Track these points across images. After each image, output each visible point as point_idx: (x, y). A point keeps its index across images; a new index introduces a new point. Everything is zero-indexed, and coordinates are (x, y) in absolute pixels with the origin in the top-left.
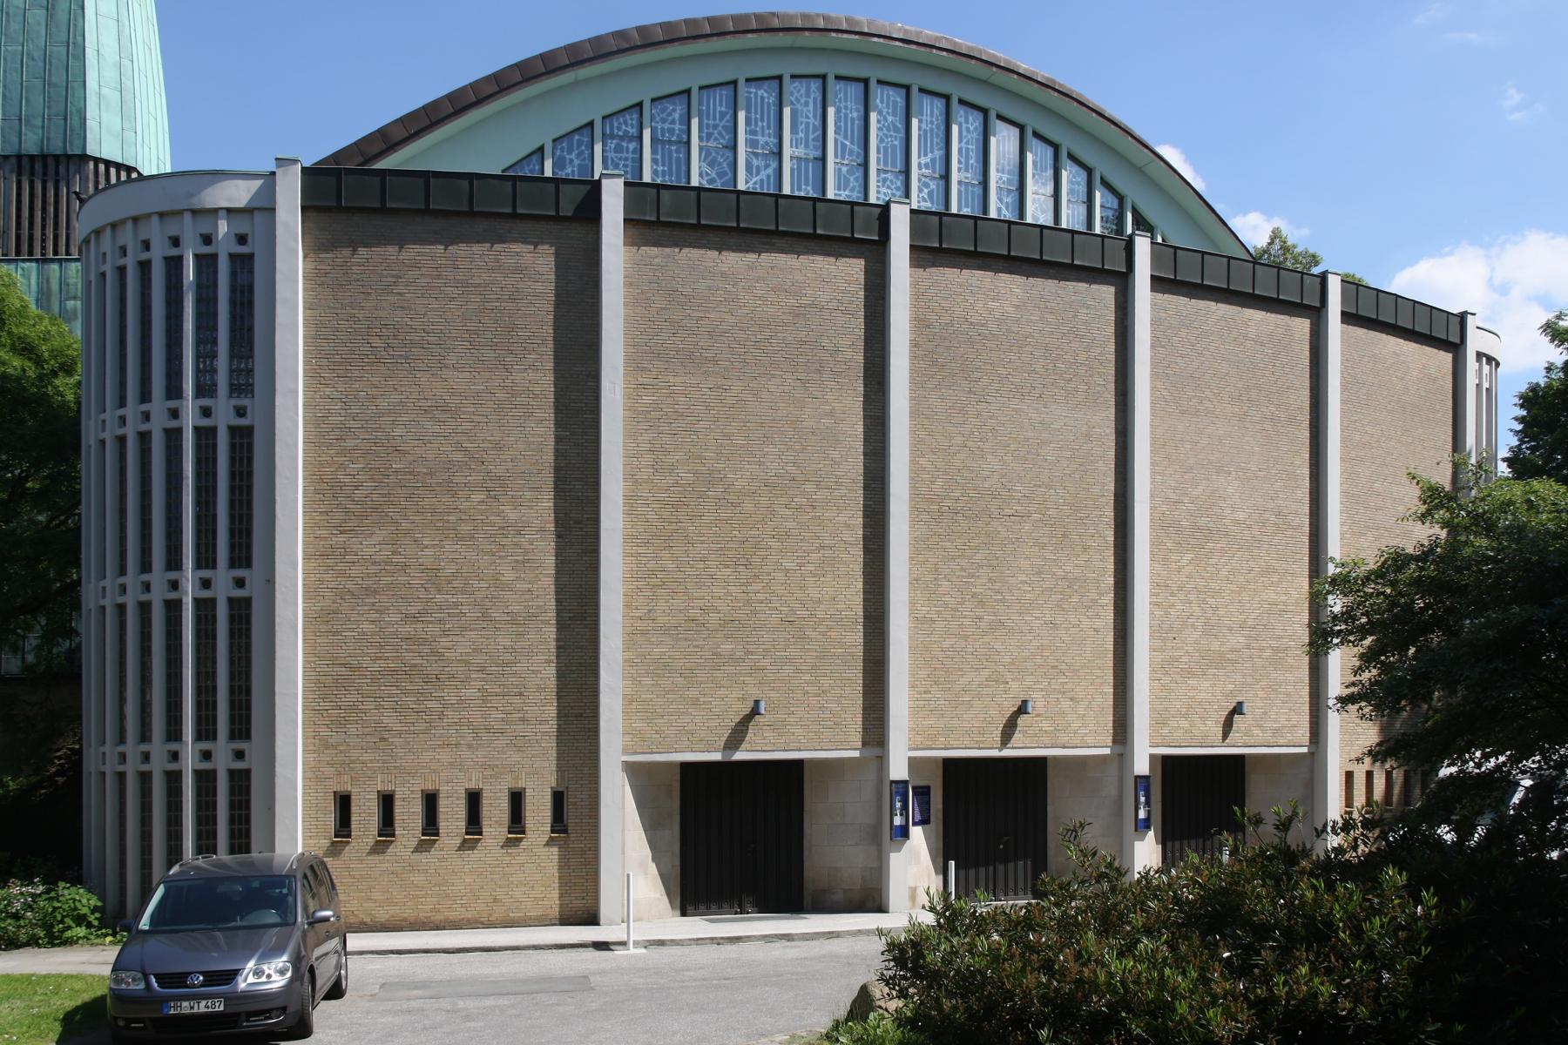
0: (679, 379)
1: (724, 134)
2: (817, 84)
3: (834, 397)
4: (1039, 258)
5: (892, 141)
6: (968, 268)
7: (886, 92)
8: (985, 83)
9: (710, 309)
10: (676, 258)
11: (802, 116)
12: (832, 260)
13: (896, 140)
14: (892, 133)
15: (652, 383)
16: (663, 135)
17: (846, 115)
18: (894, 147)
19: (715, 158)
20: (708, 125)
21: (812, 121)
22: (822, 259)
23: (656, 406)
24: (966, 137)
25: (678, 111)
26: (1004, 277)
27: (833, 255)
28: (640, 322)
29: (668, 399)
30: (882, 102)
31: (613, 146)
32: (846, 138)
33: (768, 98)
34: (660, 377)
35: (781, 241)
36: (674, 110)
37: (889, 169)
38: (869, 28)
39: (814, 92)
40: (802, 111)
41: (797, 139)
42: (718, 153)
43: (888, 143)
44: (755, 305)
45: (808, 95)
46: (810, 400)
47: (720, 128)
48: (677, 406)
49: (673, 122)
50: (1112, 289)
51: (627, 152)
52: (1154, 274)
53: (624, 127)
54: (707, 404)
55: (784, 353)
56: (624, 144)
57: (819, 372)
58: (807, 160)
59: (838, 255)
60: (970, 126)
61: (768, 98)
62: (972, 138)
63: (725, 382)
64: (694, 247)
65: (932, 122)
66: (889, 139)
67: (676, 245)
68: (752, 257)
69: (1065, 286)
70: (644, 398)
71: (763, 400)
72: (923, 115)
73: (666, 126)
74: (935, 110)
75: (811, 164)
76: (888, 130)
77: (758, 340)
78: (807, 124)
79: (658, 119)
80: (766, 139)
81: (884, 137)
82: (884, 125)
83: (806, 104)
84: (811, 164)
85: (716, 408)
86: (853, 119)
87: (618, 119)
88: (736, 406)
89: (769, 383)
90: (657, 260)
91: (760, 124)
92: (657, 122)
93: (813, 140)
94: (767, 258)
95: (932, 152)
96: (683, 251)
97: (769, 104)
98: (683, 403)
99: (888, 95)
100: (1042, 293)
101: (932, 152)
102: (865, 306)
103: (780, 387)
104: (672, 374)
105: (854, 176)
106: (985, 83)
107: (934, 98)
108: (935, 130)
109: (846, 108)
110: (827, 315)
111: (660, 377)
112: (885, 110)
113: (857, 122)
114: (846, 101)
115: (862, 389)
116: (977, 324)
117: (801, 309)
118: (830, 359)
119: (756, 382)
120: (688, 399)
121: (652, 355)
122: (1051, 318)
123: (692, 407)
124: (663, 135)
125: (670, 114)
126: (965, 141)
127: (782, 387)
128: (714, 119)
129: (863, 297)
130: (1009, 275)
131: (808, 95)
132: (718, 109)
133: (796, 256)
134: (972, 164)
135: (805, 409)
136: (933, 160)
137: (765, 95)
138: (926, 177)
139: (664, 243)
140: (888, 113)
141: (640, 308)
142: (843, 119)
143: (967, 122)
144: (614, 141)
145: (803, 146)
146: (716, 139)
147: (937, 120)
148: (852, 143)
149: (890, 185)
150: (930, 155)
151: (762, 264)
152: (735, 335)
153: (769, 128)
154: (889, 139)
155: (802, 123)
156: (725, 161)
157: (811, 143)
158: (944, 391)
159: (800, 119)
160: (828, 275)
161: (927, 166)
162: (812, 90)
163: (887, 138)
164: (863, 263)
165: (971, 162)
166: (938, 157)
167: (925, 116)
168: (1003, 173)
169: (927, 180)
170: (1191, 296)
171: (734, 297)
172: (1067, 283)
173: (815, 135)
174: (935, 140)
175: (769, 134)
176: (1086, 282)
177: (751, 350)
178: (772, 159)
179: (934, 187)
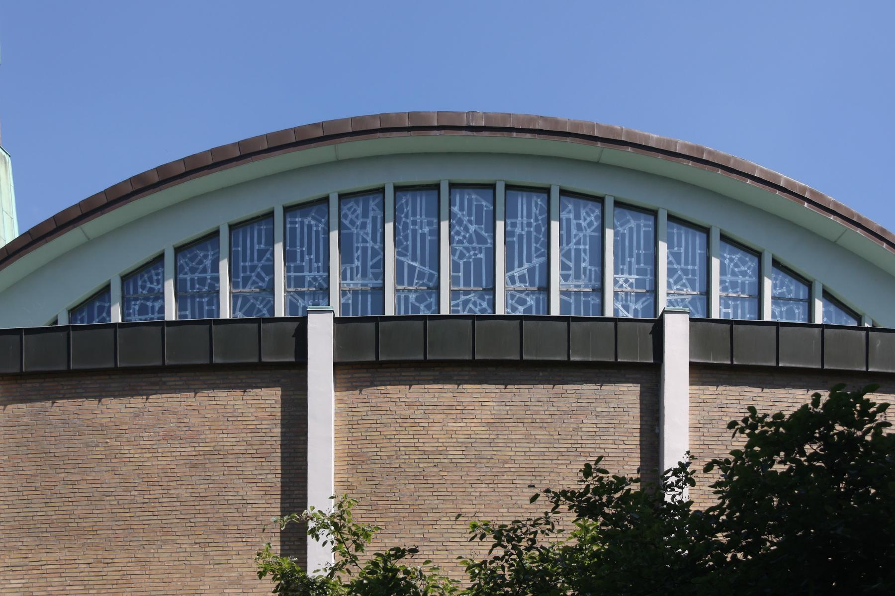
0: (52, 557)
1: (263, 275)
2: (377, 201)
3: (241, 561)
4: (518, 358)
5: (475, 254)
6: (419, 383)
7: (467, 197)
8: (596, 165)
9: (88, 470)
10: (47, 413)
11: (358, 242)
12: (239, 393)
13: (481, 253)
14: (475, 245)
15: (22, 564)
16: (193, 287)
17: (414, 232)
18: (478, 262)
19: (253, 305)
20: (244, 268)
21: (370, 244)
22: (225, 394)
23: (26, 589)
24: (576, 235)
25: (210, 257)
26: (472, 390)
27: (239, 388)
28: (8, 494)
29: (40, 580)
30: (462, 209)
31: (137, 308)
32: (414, 259)
33: (317, 226)
34: (30, 556)
35: (173, 379)
36: (206, 257)
37: (472, 287)
38: (717, 161)
39: (373, 210)
40: (358, 234)
41: (352, 269)
42: (257, 299)
43: (470, 257)
44: (143, 459)
45: (365, 215)
46: (212, 566)
47: (259, 270)
48: (49, 589)
49: (204, 271)
50: (636, 388)
51: (153, 313)
52: (693, 360)
53: (148, 285)
54: (86, 583)
55: (178, 513)
56: (149, 304)
57: (222, 532)
58: (364, 293)
59: (245, 387)
60: (581, 221)
61: (317, 226)
62: (585, 236)
63: (106, 554)
64: (68, 398)
65: (529, 225)
66: (472, 253)
67: (47, 399)
68: (137, 402)
69: (562, 391)
70: (12, 581)
71: (154, 572)
72: (517, 218)
73: (197, 276)
74: (534, 209)
75: (369, 296)
76: (470, 241)
77: (147, 501)
78: (365, 250)
79: (187, 269)
80: (315, 273)
81: (465, 252)
82: (464, 237)
83: (364, 226)
84: (369, 296)
85: (96, 587)
86: (423, 236)
87: (142, 276)
88: (120, 582)
89: (160, 551)
90: (25, 419)
91: (306, 257)
92: (186, 274)
93: (372, 267)
94: (157, 401)
95: (529, 260)
96: (55, 405)
97: (317, 232)
98: (56, 584)
99: (470, 201)
100: (528, 404)
101: (529, 260)
102: (281, 445)
103: (173, 555)
104: (44, 551)
105: (425, 303)
106: (596, 165)
107: (533, 194)
108: (534, 233)
109: (414, 223)
110: (231, 459)
111: (30, 556)
112: (466, 219)
113: (428, 238)
114: (414, 214)
115: (279, 547)
116: (433, 453)
117: (199, 457)
118: (237, 514)
119: (144, 551)
120: (63, 579)
121: (22, 531)
122: (541, 434)
123: (68, 588)
124: (193, 287)
125: (200, 262)
126: (574, 241)
127: (177, 555)
128: (252, 260)
129: (279, 434)
130: (479, 386)
131: (365, 215)
132: (256, 247)
133: (192, 394)
134: (585, 268)
135: (206, 579)
136: (531, 271)
137: (313, 222)
138: (521, 292)
139: (34, 397)
140: (470, 222)
141: (6, 478)
142: (410, 238)
143: (577, 217)
144: (138, 302)
145: (359, 276)
146: (254, 283)
147: (536, 220)
148: (423, 263)
149: (473, 307)
150: (526, 265)
151: (151, 409)
152: (118, 498)
153: (317, 261)
154: (472, 253)
155: (357, 248)
156: (264, 307)
157: (370, 271)
158: (386, 540)
159: (355, 245)
160: (234, 412)
161: (522, 279)
162: (370, 208)
163: (469, 251)
164: (279, 393)
165: (583, 265)
166: (537, 265)
167: (520, 218)
168: (630, 274)
169: (523, 296)
170: (763, 385)
171: (117, 452)
172: (565, 387)
173: (375, 261)
174: (534, 245)
175: (318, 267)
176: (595, 382)
177: (138, 514)
178: (321, 297)
179: (533, 303)
